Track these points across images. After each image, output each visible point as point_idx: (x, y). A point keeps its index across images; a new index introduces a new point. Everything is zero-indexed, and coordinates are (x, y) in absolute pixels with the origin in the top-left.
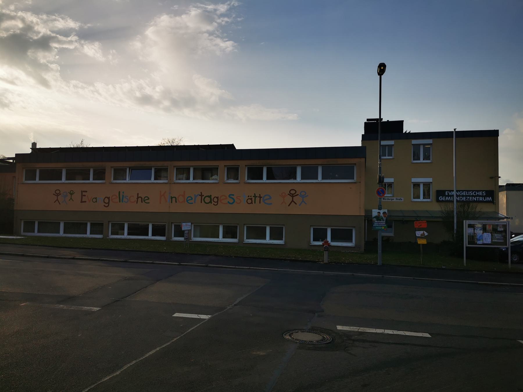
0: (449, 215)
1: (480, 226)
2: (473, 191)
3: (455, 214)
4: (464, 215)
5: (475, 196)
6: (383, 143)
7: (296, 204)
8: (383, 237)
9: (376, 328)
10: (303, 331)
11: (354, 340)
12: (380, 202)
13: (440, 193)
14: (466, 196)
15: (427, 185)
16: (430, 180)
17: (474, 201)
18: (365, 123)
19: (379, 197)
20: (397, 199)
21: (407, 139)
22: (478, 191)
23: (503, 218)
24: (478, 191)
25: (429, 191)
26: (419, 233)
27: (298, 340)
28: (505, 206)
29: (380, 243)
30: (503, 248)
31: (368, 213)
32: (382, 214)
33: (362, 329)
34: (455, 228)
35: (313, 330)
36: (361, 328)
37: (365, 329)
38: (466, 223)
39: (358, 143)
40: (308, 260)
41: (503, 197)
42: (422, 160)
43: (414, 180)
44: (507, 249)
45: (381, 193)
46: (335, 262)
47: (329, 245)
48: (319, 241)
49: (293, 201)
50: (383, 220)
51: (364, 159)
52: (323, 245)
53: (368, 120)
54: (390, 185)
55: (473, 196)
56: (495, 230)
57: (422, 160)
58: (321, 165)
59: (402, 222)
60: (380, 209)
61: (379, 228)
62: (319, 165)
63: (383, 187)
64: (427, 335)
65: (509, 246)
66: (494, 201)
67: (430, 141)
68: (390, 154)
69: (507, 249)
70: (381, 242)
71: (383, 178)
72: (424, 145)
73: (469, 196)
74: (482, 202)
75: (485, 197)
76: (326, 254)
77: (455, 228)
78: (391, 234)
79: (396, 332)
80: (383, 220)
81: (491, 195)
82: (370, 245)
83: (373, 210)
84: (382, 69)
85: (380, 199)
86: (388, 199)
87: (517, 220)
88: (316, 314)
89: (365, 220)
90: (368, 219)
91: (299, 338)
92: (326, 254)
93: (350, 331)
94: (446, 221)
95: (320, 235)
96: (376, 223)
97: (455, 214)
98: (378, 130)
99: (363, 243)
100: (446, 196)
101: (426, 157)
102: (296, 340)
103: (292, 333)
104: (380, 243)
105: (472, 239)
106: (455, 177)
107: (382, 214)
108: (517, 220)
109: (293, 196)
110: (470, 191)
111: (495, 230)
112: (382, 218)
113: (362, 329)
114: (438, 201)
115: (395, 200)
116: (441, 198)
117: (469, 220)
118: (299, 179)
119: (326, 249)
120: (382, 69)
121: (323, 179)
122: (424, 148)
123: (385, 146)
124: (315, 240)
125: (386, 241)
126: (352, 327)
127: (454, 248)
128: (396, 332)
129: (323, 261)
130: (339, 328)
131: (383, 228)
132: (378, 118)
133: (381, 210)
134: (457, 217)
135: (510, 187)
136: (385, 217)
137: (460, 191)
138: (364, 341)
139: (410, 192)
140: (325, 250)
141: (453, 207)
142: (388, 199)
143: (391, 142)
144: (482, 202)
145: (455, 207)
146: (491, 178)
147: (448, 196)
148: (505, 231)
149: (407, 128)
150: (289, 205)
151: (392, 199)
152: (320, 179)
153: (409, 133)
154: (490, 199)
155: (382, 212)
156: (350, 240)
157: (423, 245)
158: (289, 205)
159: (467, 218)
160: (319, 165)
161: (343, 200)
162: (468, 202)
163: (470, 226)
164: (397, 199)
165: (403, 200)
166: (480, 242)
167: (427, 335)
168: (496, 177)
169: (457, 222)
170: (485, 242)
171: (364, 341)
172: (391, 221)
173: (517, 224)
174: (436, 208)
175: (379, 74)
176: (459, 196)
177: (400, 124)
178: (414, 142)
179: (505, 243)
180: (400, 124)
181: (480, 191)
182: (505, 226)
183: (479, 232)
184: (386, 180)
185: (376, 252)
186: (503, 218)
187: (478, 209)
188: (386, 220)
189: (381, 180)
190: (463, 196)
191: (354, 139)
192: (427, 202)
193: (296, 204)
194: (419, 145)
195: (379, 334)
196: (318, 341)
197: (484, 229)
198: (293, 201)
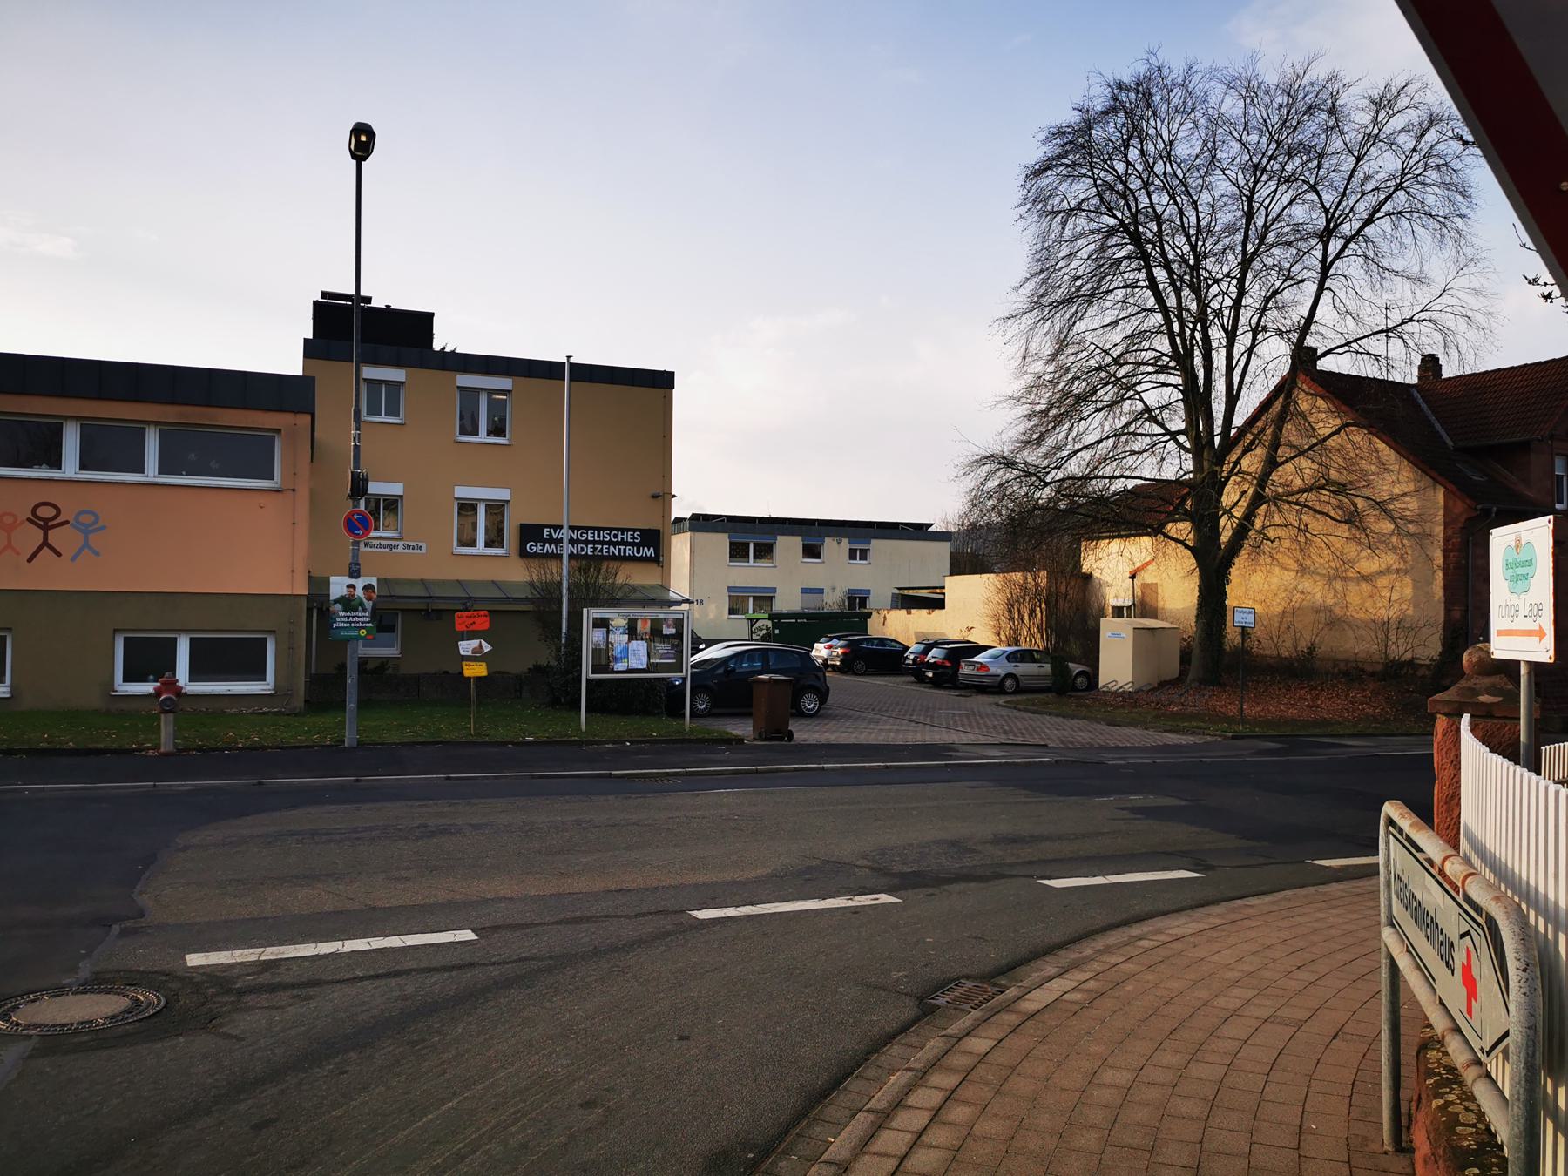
0: (546, 597)
1: (623, 623)
2: (611, 530)
3: (565, 592)
4: (588, 594)
5: (615, 544)
6: (370, 372)
7: (59, 554)
8: (363, 662)
9: (293, 941)
10: (57, 991)
11: (241, 993)
12: (356, 553)
13: (530, 532)
14: (594, 542)
15: (496, 510)
16: (502, 494)
17: (613, 558)
18: (315, 303)
19: (351, 539)
20: (406, 547)
21: (444, 368)
22: (623, 531)
23: (679, 603)
24: (623, 531)
25: (500, 531)
26: (466, 647)
27: (36, 1026)
28: (686, 570)
29: (351, 679)
30: (674, 676)
31: (319, 585)
32: (359, 593)
33: (270, 953)
34: (564, 629)
35: (98, 983)
36: (270, 950)
37: (282, 948)
38: (590, 614)
39: (292, 365)
40: (101, 746)
41: (680, 547)
42: (482, 437)
43: (463, 492)
44: (684, 679)
45: (357, 526)
46: (199, 749)
47: (179, 692)
48: (146, 681)
49: (45, 543)
50: (364, 610)
51: (309, 418)
52: (158, 693)
53: (324, 295)
54: (392, 504)
55: (610, 543)
56: (656, 633)
57: (482, 437)
58: (156, 423)
59: (416, 613)
60: (355, 574)
61: (352, 633)
62: (149, 423)
63: (368, 513)
64: (468, 935)
65: (687, 672)
66: (659, 559)
67: (505, 383)
68: (393, 411)
69: (684, 679)
70: (355, 676)
71: (366, 481)
72: (491, 392)
73: (603, 543)
74: (633, 559)
75: (638, 545)
76: (166, 727)
77: (564, 629)
78: (393, 652)
79: (377, 943)
80: (364, 610)
81: (653, 541)
82: (323, 691)
83: (333, 579)
84: (362, 142)
85: (357, 544)
86: (381, 546)
87: (713, 606)
88: (116, 928)
89: (309, 611)
90: (318, 603)
91: (39, 1020)
92: (166, 727)
93: (232, 966)
94: (543, 615)
95: (149, 658)
96: (341, 618)
97: (565, 592)
98: (355, 330)
99: (301, 681)
100: (545, 541)
101: (497, 430)
102: (27, 1027)
103: (16, 1007)
104: (351, 679)
105: (603, 660)
106: (560, 489)
107: (359, 593)
108: (713, 606)
109: (46, 526)
110: (604, 529)
111: (656, 633)
112: (361, 604)
113: (270, 953)
114: (523, 554)
115: (400, 550)
116: (532, 547)
117: (598, 606)
118: (70, 466)
119: (169, 708)
120: (362, 142)
121: (162, 470)
122: (490, 402)
123: (374, 384)
124: (128, 678)
125: (373, 673)
126: (238, 952)
127: (554, 684)
128: (377, 943)
129: (157, 747)
130: (194, 960)
131: (363, 633)
132: (352, 291)
133: (357, 577)
134: (569, 600)
135: (702, 523)
136: (369, 599)
137: (579, 528)
138: (273, 988)
139: (446, 526)
140: (166, 712)
141: (561, 575)
142: (381, 546)
143: (397, 374)
144: (633, 559)
145: (565, 572)
146: (655, 497)
147: (551, 541)
148: (679, 636)
149: (444, 338)
150: (30, 560)
151: (392, 547)
152: (151, 472)
153: (453, 352)
154: (650, 552)
155: (360, 583)
156: (260, 675)
157: (479, 679)
158: (30, 560)
159: (595, 603)
160: (149, 423)
161: (241, 545)
162: (599, 559)
163: (602, 623)
164: (406, 547)
165: (424, 551)
166: (619, 666)
167: (468, 935)
168: (663, 496)
169: (569, 613)
170: (635, 666)
171: (273, 988)
172: (394, 609)
173: (711, 616)
174: (516, 574)
175: (354, 156)
176: (578, 542)
177: (424, 321)
178: (465, 380)
179: (678, 667)
180: (424, 321)
181: (628, 530)
182: (679, 623)
183: (619, 639)
184: (374, 488)
185: (342, 706)
186: (679, 603)
187: (620, 579)
188: (374, 609)
189: (359, 487)
190: (587, 542)
191: (283, 353)
192: (496, 556)
193: (59, 554)
194: (477, 390)
195: (326, 956)
196: (111, 1018)
197: (632, 632)
198: (45, 543)
